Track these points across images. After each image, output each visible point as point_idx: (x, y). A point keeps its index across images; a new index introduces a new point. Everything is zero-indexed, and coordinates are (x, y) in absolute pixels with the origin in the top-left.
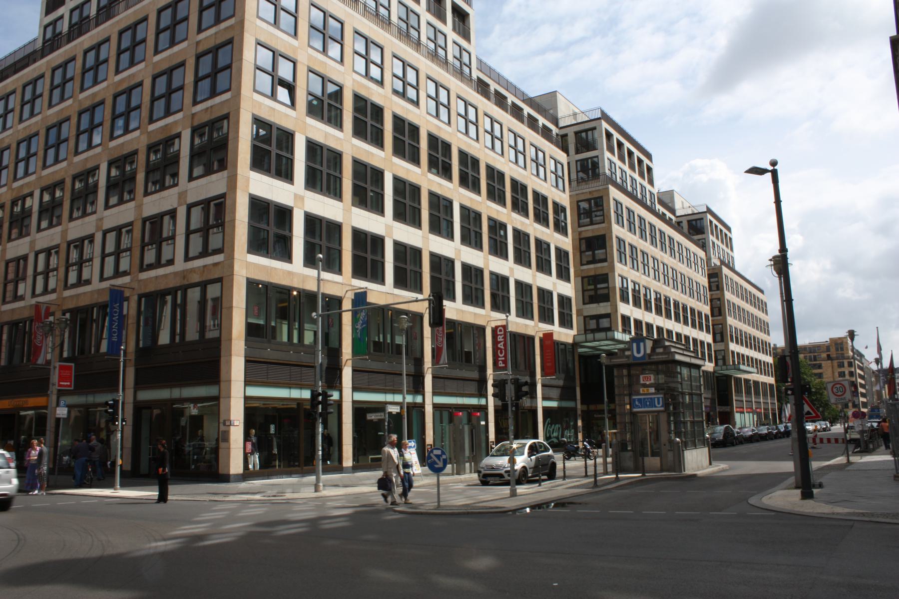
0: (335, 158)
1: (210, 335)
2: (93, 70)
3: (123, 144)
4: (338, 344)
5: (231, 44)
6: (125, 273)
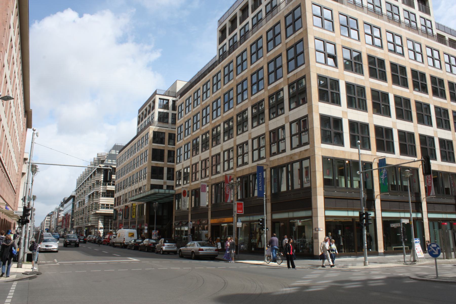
0: (361, 90)
1: (306, 185)
2: (241, 65)
3: (257, 97)
4: (371, 187)
5: (302, 41)
6: (263, 158)
